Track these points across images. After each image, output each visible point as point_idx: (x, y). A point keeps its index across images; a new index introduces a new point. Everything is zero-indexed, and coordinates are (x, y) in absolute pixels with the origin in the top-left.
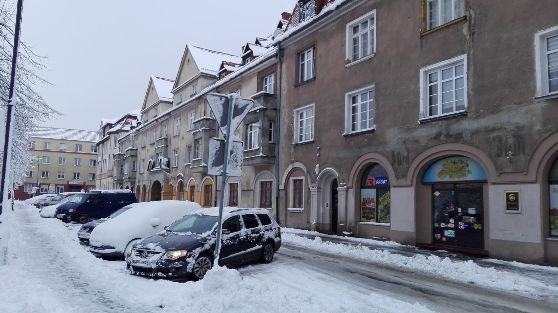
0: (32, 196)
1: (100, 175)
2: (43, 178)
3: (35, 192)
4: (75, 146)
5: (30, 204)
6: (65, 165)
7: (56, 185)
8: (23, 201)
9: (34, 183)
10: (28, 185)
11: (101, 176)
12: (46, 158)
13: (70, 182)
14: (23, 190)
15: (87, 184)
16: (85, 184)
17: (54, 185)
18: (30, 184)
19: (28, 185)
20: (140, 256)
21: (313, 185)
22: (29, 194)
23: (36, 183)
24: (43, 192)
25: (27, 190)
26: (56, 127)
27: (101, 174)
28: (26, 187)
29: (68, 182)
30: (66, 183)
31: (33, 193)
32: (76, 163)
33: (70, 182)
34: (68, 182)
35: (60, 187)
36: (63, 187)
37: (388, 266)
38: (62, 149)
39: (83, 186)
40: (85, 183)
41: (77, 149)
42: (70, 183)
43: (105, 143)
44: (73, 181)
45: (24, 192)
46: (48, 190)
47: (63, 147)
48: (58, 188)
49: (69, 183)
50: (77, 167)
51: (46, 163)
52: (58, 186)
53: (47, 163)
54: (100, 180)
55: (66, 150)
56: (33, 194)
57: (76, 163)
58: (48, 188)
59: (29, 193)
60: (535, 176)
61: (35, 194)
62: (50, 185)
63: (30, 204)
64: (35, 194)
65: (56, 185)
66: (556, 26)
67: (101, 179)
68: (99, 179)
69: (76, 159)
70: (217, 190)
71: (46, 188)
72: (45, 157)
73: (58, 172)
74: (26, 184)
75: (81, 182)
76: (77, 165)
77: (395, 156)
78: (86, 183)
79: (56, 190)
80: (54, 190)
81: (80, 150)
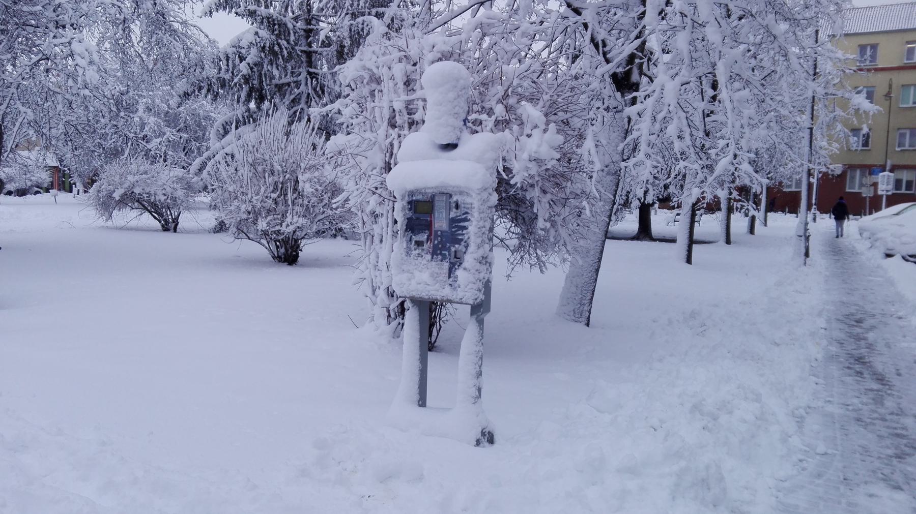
0: (875, 205)
2: (902, 150)
3: (887, 191)
8: (788, 215)
10: (858, 172)
12: (912, 89)
14: (844, 187)
18: (863, 167)
19: (858, 172)
20: (181, 98)
21: (790, 183)
22: (865, 198)
23: (881, 166)
24: (900, 190)
25: (856, 185)
28: (853, 178)
31: (880, 193)
45: (848, 190)
51: (911, 105)
56: (882, 196)
59: (867, 193)
61: (888, 196)
64: (888, 196)
70: (695, 237)
71: (909, 179)
72: (909, 86)
73: (170, 226)
74: (851, 167)
77: (859, 341)
81: (873, 57)
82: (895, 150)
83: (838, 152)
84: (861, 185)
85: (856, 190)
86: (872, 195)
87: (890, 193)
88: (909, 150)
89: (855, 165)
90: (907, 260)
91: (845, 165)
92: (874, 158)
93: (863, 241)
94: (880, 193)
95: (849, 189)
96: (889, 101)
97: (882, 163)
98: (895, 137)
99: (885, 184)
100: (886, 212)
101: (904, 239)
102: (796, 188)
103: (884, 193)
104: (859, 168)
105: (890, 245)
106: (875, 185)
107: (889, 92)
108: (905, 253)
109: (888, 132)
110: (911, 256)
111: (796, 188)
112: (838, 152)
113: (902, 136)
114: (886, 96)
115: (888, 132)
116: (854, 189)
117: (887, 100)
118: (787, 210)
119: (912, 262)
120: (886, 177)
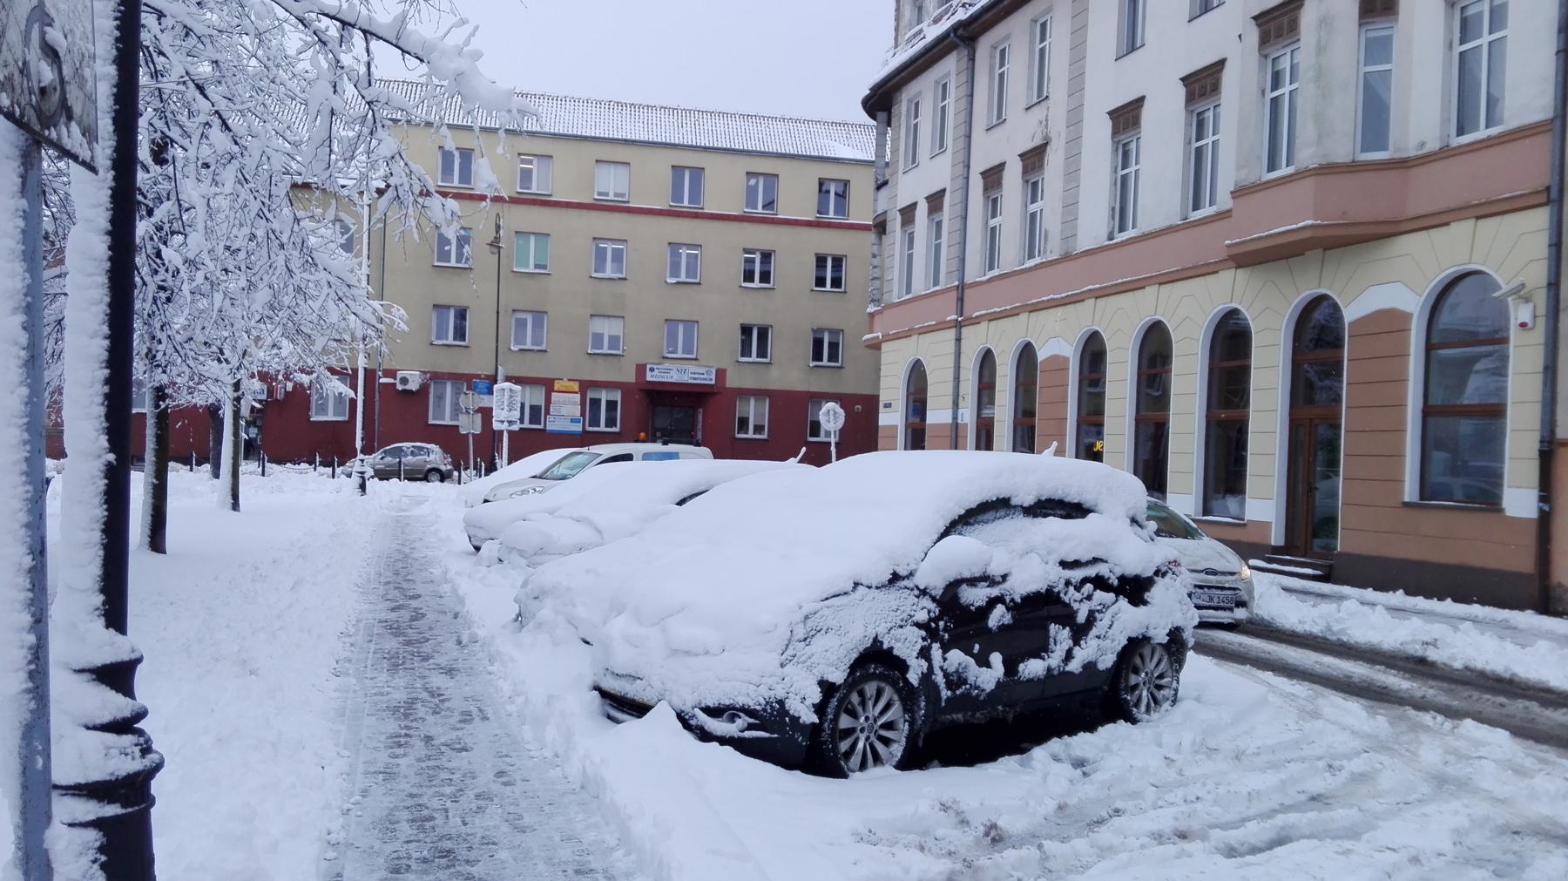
1: (954, 295)
2: (521, 350)
3: (510, 422)
4: (668, 175)
5: (662, 719)
6: (625, 279)
7: (585, 386)
8: (321, 469)
9: (478, 376)
11: (961, 300)
13: (652, 370)
15: (732, 382)
16: (724, 383)
17: (576, 387)
18: (456, 378)
22: (466, 436)
23: (487, 377)
26: (562, 95)
27: (962, 288)
29: (641, 369)
30: (630, 377)
32: (675, 271)
33: (652, 370)
34: (641, 369)
35: (604, 396)
36: (617, 396)
37: (1498, 675)
38: (607, 194)
39: (714, 393)
40: (721, 374)
41: (677, 194)
42: (649, 377)
43: (984, 44)
44: (667, 365)
46: (547, 412)
47: (611, 183)
48: (596, 403)
49: (649, 374)
50: (683, 289)
51: (531, 269)
52: (590, 395)
53: (537, 266)
54: (952, 333)
55: (622, 195)
57: (675, 271)
58: (548, 401)
60: (950, 412)
62: (557, 386)
63: (662, 719)
65: (585, 386)
66: (152, 515)
67: (958, 325)
68: (941, 326)
69: (674, 246)
74: (437, 377)
75: (703, 370)
76: (683, 278)
78: (729, 374)
79: (583, 414)
80: (577, 411)
82: (510, 349)
83: (406, 328)
84: (457, 411)
85: (447, 421)
86: (478, 432)
87: (516, 427)
88: (532, 350)
89: (443, 374)
90: (704, 736)
91: (425, 373)
92: (477, 362)
93: (483, 569)
94: (496, 426)
95: (434, 419)
96: (497, 256)
97: (490, 372)
98: (508, 323)
99: (506, 408)
100: (511, 473)
101: (684, 632)
102: (531, 423)
103: (505, 426)
104: (449, 379)
105: (623, 659)
106: (486, 413)
107: (496, 238)
108: (687, 702)
109: (498, 313)
110: (714, 712)
111: (531, 423)
112: (406, 328)
113: (521, 324)
114: (491, 245)
115: (498, 313)
116: (443, 419)
117: (493, 253)
118: (318, 459)
119: (723, 741)
120: (507, 393)
